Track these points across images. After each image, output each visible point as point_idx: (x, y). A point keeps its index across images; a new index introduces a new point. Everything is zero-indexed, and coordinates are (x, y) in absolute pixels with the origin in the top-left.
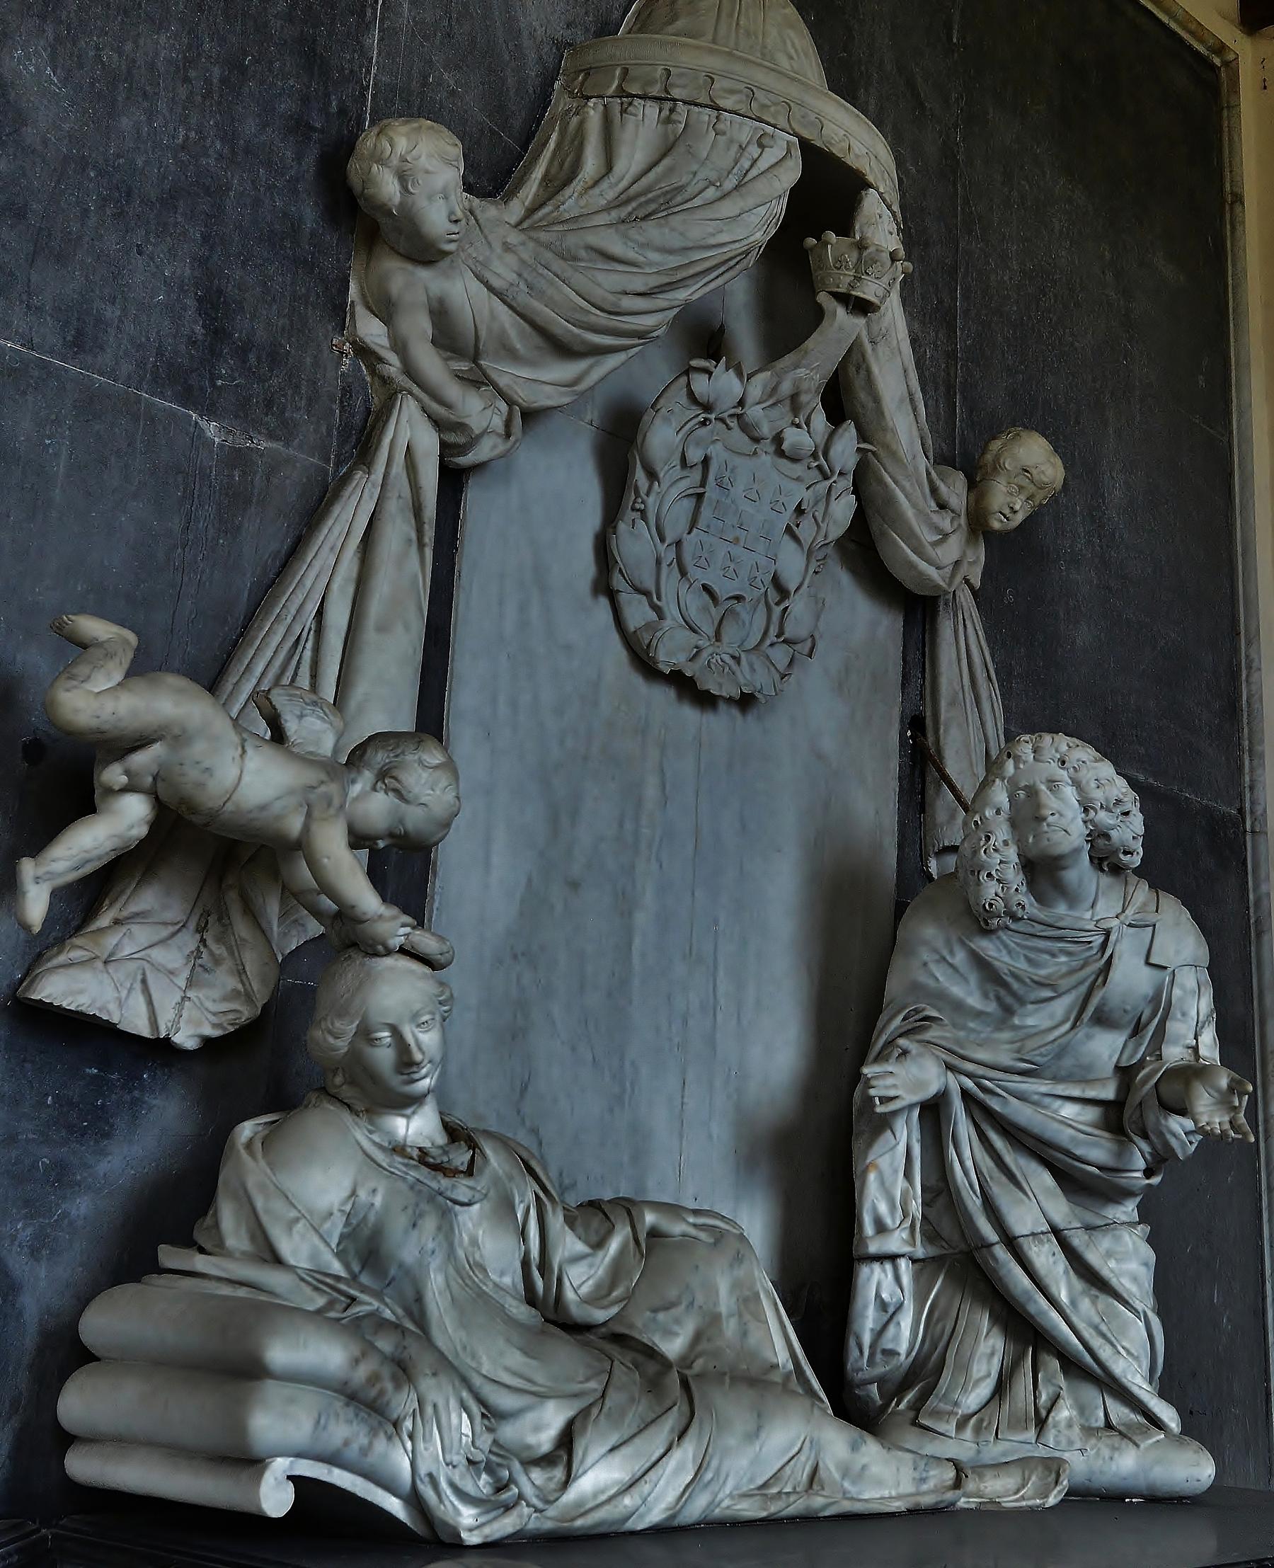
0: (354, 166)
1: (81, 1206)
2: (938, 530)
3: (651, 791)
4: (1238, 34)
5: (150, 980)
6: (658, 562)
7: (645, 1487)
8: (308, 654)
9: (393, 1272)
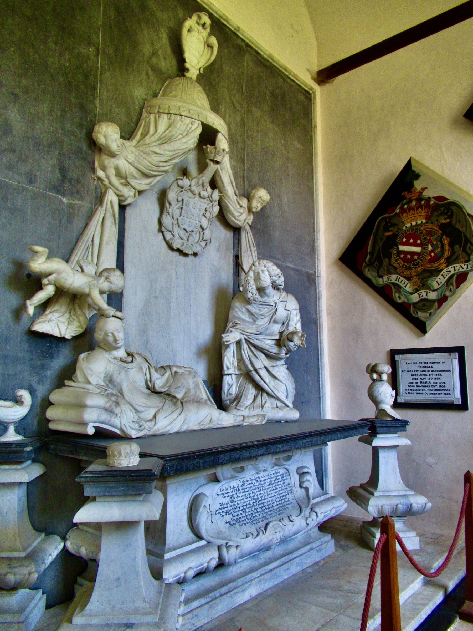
0: (94, 135)
1: (49, 373)
2: (239, 212)
3: (174, 275)
4: (317, 85)
5: (58, 324)
6: (173, 224)
7: (172, 425)
8: (90, 250)
9: (115, 384)
